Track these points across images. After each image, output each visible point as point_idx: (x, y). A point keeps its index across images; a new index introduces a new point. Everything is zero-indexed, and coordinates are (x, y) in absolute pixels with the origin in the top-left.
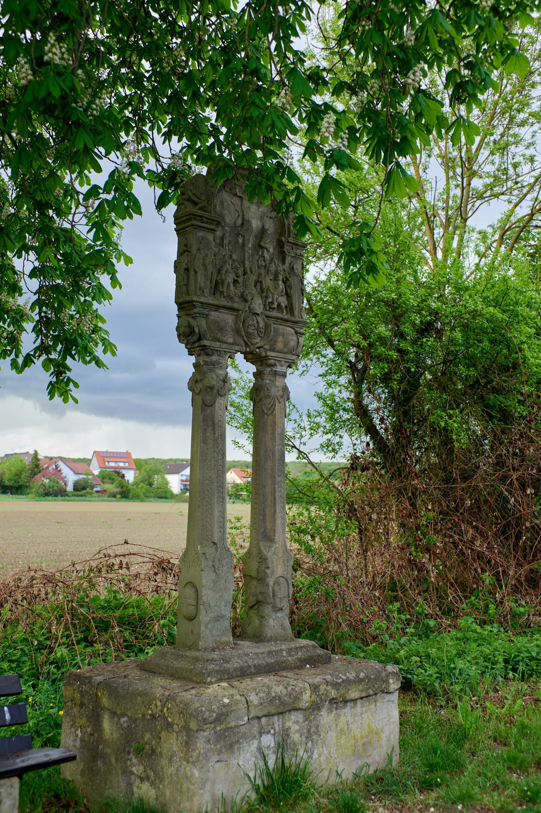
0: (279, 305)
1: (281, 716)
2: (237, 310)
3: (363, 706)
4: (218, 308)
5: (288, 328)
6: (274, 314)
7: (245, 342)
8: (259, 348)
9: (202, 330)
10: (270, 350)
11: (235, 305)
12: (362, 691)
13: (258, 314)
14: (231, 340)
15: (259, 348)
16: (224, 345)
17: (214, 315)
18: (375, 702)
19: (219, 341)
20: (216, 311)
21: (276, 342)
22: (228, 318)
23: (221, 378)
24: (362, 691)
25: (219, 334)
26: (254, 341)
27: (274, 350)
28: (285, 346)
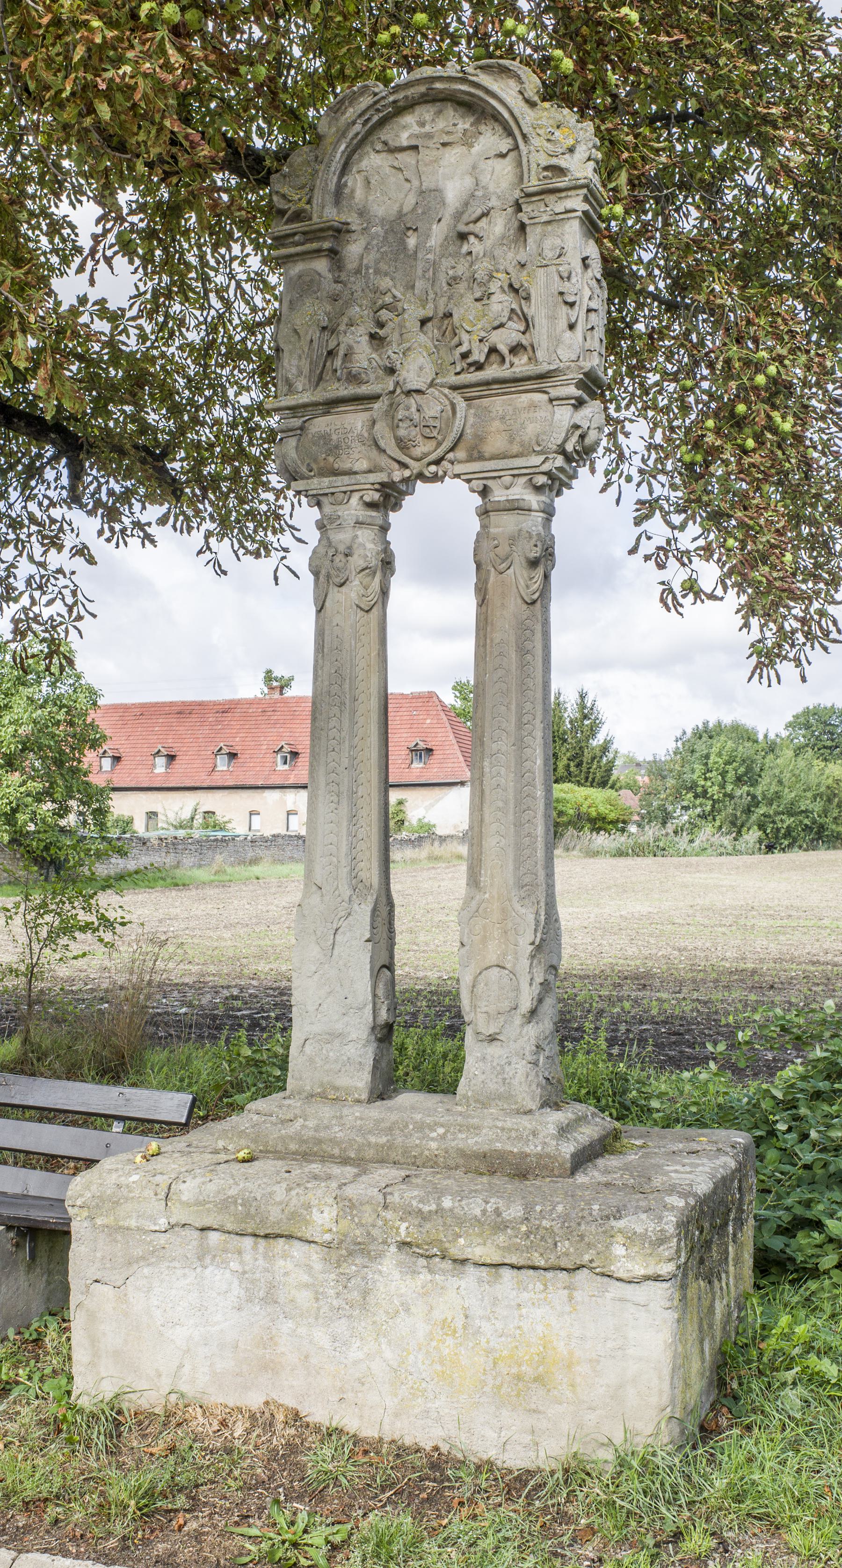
0: (493, 350)
1: (262, 1242)
2: (376, 397)
3: (521, 1287)
4: (331, 405)
5: (525, 397)
6: (492, 372)
7: (399, 462)
8: (437, 462)
9: (288, 462)
10: (470, 459)
11: (364, 390)
12: (507, 1249)
13: (418, 391)
14: (363, 465)
15: (437, 462)
16: (346, 479)
17: (320, 424)
18: (569, 1287)
19: (336, 473)
20: (327, 413)
21: (480, 439)
22: (355, 421)
23: (342, 548)
24: (507, 1249)
25: (331, 459)
26: (417, 452)
27: (481, 458)
28: (511, 440)
